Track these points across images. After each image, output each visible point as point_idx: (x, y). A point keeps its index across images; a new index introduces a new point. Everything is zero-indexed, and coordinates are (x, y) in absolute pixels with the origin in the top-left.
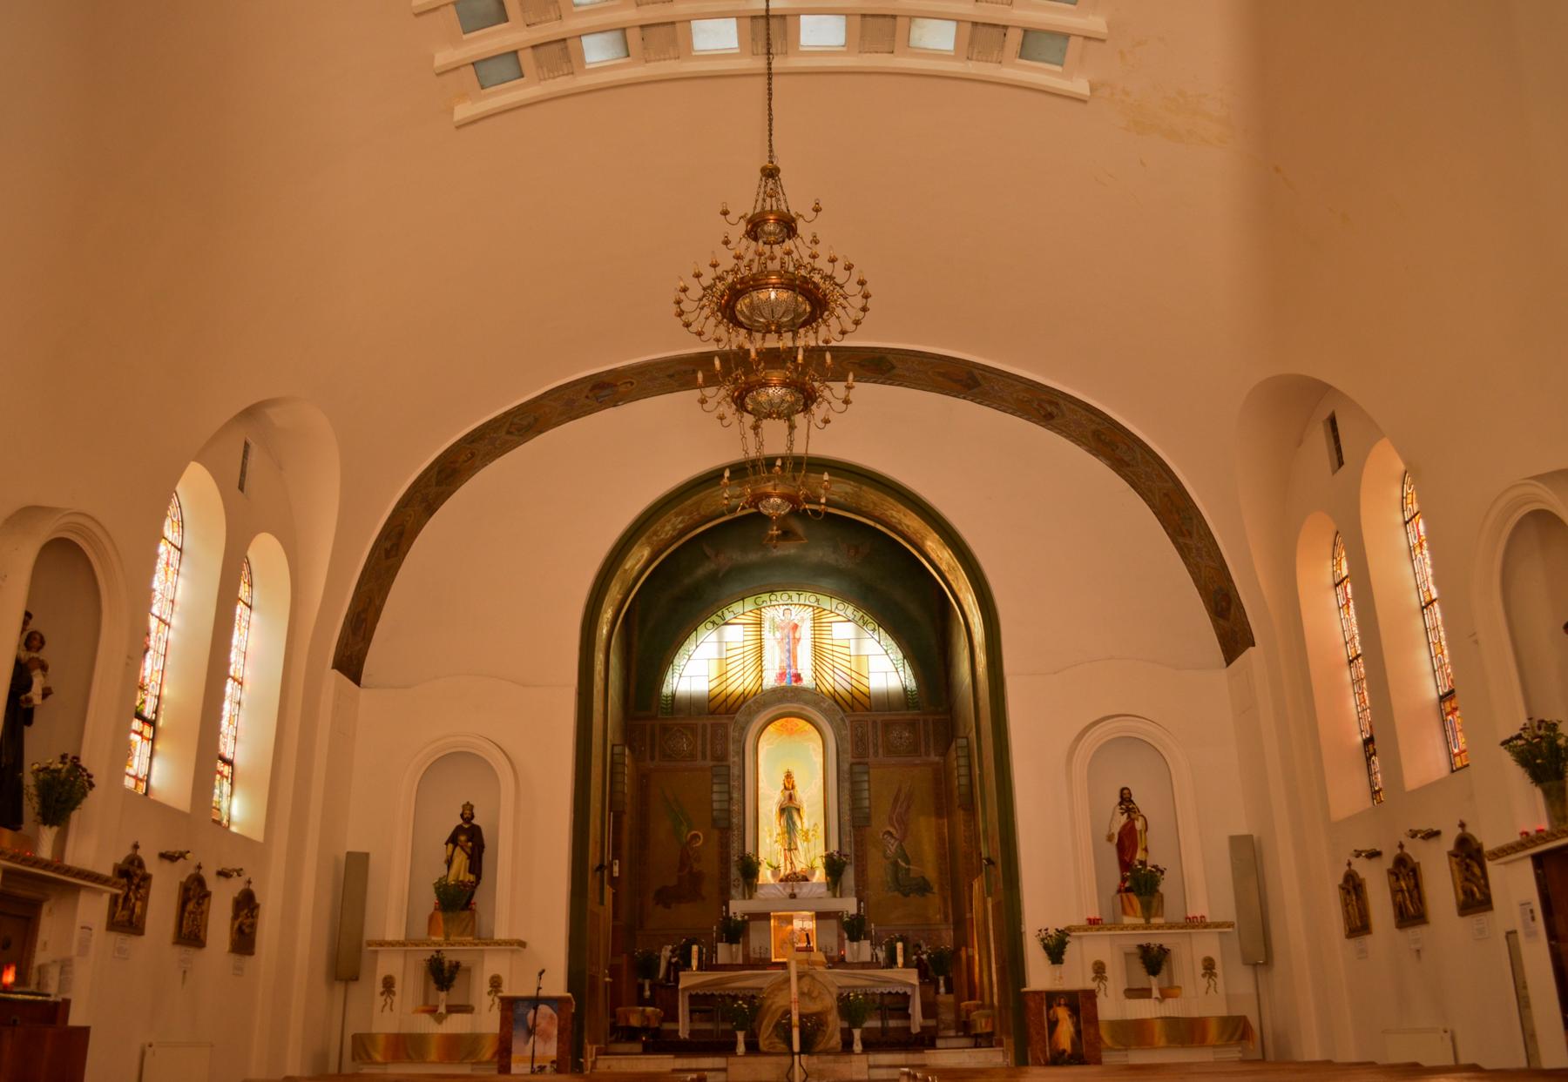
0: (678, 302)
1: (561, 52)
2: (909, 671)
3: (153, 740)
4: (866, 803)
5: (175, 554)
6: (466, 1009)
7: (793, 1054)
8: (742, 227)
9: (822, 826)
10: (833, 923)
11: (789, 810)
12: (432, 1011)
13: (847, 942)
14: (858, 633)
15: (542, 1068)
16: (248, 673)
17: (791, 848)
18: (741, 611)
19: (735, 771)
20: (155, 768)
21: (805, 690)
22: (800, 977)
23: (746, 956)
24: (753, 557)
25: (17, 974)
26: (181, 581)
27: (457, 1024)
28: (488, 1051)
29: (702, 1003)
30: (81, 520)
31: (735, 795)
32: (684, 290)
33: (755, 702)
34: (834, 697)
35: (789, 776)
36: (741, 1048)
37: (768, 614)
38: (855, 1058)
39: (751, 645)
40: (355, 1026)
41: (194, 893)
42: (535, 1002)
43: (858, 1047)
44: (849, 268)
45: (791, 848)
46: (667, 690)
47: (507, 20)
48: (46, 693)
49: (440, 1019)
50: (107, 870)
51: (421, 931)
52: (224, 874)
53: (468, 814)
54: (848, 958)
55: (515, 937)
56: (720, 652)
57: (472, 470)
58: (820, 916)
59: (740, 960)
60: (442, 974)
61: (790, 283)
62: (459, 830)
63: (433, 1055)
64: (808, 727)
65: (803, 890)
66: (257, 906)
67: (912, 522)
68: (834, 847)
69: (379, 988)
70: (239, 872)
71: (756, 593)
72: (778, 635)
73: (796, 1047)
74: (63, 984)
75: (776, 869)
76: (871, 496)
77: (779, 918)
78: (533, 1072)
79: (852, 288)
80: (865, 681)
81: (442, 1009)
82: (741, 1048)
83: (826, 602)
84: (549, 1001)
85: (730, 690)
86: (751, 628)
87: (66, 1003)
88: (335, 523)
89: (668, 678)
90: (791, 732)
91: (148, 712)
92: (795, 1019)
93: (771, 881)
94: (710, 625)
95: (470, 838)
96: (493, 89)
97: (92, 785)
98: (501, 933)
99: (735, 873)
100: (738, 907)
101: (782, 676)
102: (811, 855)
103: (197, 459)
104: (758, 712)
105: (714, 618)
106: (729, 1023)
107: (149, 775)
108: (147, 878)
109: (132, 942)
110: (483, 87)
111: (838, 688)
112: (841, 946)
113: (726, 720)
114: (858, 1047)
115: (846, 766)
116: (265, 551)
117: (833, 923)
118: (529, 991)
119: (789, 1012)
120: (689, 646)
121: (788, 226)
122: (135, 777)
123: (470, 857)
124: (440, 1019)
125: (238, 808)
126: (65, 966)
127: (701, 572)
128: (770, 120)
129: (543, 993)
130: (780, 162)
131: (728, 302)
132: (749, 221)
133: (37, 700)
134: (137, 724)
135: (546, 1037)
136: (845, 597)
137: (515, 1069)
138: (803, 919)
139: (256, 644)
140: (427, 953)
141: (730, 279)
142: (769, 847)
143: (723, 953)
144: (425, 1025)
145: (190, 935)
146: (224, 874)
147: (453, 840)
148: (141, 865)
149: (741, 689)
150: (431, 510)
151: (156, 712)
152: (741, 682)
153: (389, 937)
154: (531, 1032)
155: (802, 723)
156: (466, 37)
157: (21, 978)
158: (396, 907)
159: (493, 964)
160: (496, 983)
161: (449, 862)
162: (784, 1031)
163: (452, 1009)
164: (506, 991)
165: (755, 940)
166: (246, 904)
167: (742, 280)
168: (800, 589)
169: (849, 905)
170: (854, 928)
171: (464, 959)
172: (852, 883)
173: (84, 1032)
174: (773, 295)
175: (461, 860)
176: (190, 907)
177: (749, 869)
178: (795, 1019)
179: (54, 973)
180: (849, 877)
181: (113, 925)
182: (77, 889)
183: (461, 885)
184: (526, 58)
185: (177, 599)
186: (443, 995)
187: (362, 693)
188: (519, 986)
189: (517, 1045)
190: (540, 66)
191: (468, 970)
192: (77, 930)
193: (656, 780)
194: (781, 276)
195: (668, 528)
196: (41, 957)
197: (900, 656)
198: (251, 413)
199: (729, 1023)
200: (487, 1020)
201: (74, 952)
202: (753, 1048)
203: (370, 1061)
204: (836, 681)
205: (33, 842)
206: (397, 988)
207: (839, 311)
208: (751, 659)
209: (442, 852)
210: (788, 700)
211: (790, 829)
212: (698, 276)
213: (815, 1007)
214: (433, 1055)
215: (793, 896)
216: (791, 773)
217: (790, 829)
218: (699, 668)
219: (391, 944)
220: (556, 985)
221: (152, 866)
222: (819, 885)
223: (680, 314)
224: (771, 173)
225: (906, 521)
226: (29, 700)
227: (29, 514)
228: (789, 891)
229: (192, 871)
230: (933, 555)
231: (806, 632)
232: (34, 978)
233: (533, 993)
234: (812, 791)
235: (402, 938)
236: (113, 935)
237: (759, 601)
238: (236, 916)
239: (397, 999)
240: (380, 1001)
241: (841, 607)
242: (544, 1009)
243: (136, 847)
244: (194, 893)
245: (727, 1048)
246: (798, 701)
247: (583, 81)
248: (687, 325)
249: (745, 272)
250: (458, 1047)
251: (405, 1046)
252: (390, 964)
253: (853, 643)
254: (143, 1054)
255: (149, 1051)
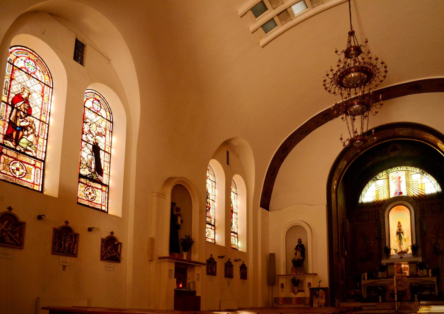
0: (324, 85)
1: (286, 14)
2: (439, 186)
3: (215, 230)
4: (425, 229)
5: (214, 184)
6: (303, 291)
7: (395, 301)
8: (343, 55)
9: (410, 237)
10: (414, 265)
11: (399, 233)
12: (293, 292)
13: (419, 270)
14: (421, 177)
15: (321, 306)
16: (238, 211)
17: (400, 244)
18: (382, 175)
19: (382, 223)
20: (214, 236)
21: (404, 197)
22: (397, 281)
23: (387, 275)
24: (385, 157)
25: (182, 285)
26: (216, 190)
27: (300, 295)
28: (308, 301)
29: (369, 288)
30: (182, 179)
31: (383, 230)
32: (325, 81)
33: (387, 202)
34: (414, 198)
35: (399, 223)
36: (380, 300)
37: (391, 175)
38: (415, 303)
39: (386, 185)
40: (275, 296)
41: (229, 266)
42: (318, 289)
43: (416, 300)
44: (377, 59)
45: (400, 244)
46: (360, 202)
47: (267, 9)
48: (181, 221)
49: (296, 294)
50: (204, 261)
51: (290, 272)
52: (236, 260)
53: (300, 241)
54: (419, 275)
55: (314, 272)
56: (376, 189)
57: (292, 147)
58: (410, 263)
59: (385, 276)
60: (296, 283)
61: (359, 69)
62: (298, 246)
63: (294, 302)
64: (405, 208)
65: (405, 256)
66: (247, 268)
67: (432, 138)
68: (414, 242)
69: (280, 286)
70: (240, 260)
71: (386, 169)
72: (394, 181)
73: (396, 300)
74: (194, 287)
75: (396, 251)
76: (417, 132)
77: (396, 264)
78: (319, 306)
79: (379, 65)
80: (424, 192)
81: (296, 291)
82: (380, 300)
83: (410, 168)
84: (323, 289)
85: (379, 199)
86: (386, 180)
87: (195, 291)
88: (254, 167)
89: (360, 198)
90: (400, 210)
91: (213, 223)
92: (396, 292)
93: (395, 254)
94: (372, 181)
95: (301, 248)
96: (269, 33)
97: (193, 242)
98: (310, 272)
99: (383, 252)
100: (384, 262)
101: (396, 193)
102: (407, 245)
103: (213, 157)
104: (389, 205)
105: (373, 178)
106: (378, 293)
107: (215, 238)
108: (216, 263)
109: (213, 277)
110: (266, 33)
111: (415, 195)
112: (417, 271)
113: (380, 208)
114: (416, 300)
115: (418, 218)
116: (237, 178)
117: (414, 265)
118: (316, 286)
119: (394, 290)
120: (366, 188)
121: (358, 50)
122: (211, 239)
123: (301, 253)
124: (296, 294)
125: (239, 244)
126: (194, 283)
127: (369, 164)
128: (350, 15)
129: (320, 287)
130: (354, 30)
131: (339, 81)
132: (345, 53)
133: (180, 223)
134: (208, 226)
135: (322, 298)
136: (416, 166)
137: (314, 306)
138: (405, 264)
139: (239, 203)
140: (291, 277)
141: (339, 73)
142: (394, 244)
143: (380, 274)
144: (292, 295)
145: (229, 274)
146: (236, 260)
147: (296, 249)
148: (213, 259)
149: (383, 199)
150: (282, 160)
151: (214, 223)
152: (383, 196)
153: (282, 274)
154: (317, 296)
155: (403, 207)
156: (257, 19)
157: (184, 286)
158: (282, 267)
159: (308, 280)
160: (309, 284)
161: (296, 254)
162: (392, 295)
163: (299, 291)
164: (312, 286)
165: (390, 271)
166: (244, 268)
167: (342, 73)
168: (401, 165)
169: (420, 259)
170: (420, 266)
171: (301, 279)
172: (421, 253)
173: (200, 297)
174: (353, 75)
175: (299, 253)
176: (228, 268)
177: (388, 250)
178: (396, 292)
179: (192, 285)
180: (420, 251)
181: (208, 274)
182: (194, 266)
183: (298, 260)
184: (276, 19)
185: (216, 194)
186: (296, 288)
187: (270, 213)
188: (315, 285)
189: (314, 300)
190: (281, 20)
191: (302, 281)
192: (196, 275)
193: (356, 227)
194: (355, 68)
195: (351, 154)
196: (188, 281)
197: (436, 182)
198: (227, 143)
199: (378, 293)
200: (307, 294)
201: (196, 280)
202: (384, 300)
203: (279, 304)
204: (414, 192)
205: (182, 256)
206: (285, 286)
207: (377, 74)
208: (386, 189)
209: (294, 252)
210: (399, 200)
211: (400, 238)
212: (328, 75)
213: (401, 289)
214: (294, 302)
215: (401, 258)
216: (400, 222)
217: (400, 238)
218: (371, 193)
219: (282, 275)
220: (325, 283)
221: (216, 259)
222: (410, 254)
223: (326, 89)
224: (352, 33)
225: (430, 138)
226: (178, 223)
227: (169, 180)
228: (400, 256)
229: (227, 260)
230: (441, 148)
231: (403, 179)
232: (188, 286)
233: (318, 287)
234: (407, 227)
235: (285, 274)
236: (208, 276)
237: (387, 171)
238: (241, 271)
239: (285, 289)
240: (280, 290)
241: (415, 169)
242: (321, 291)
243: (212, 255)
244: (229, 266)
245: (377, 300)
246: (401, 200)
247: (295, 21)
248: (330, 91)
249: (342, 71)
250: (299, 300)
251: (287, 300)
252: (282, 281)
253: (419, 180)
254: (220, 302)
255: (221, 302)
